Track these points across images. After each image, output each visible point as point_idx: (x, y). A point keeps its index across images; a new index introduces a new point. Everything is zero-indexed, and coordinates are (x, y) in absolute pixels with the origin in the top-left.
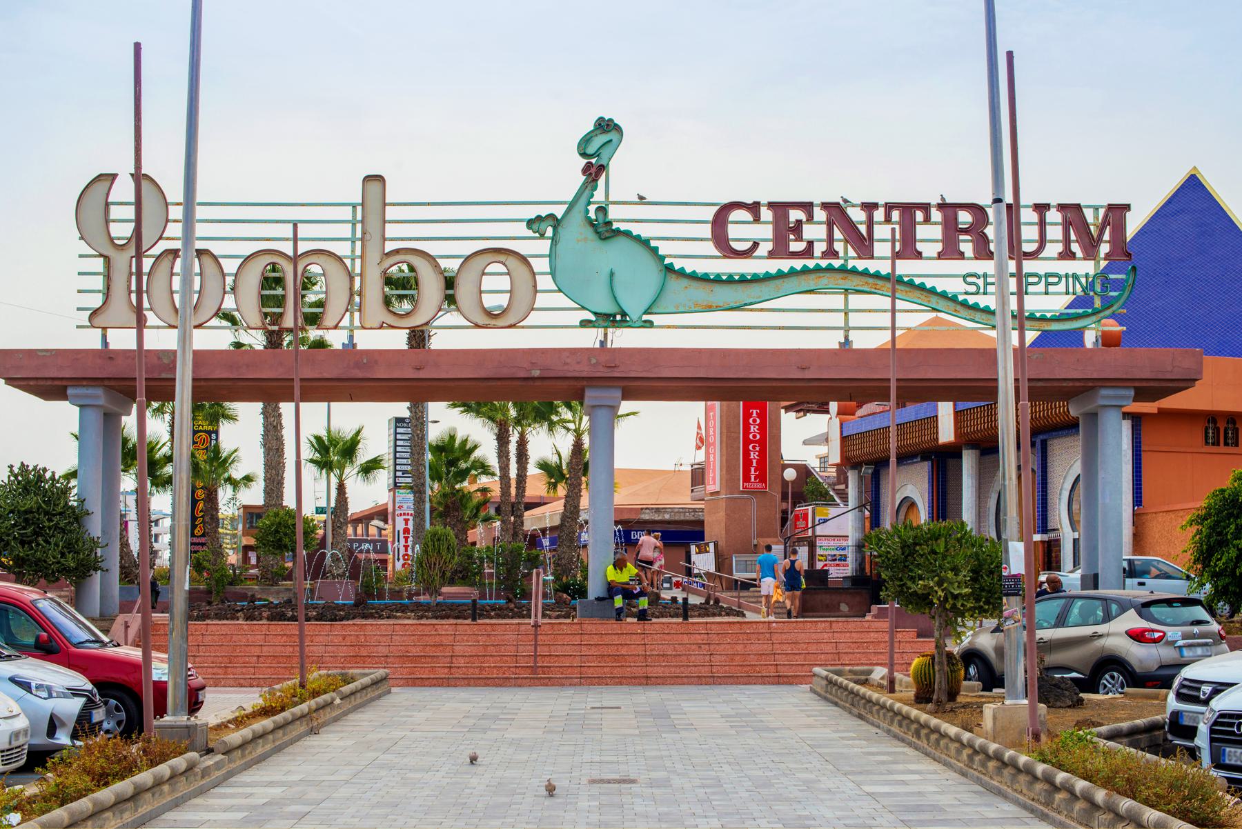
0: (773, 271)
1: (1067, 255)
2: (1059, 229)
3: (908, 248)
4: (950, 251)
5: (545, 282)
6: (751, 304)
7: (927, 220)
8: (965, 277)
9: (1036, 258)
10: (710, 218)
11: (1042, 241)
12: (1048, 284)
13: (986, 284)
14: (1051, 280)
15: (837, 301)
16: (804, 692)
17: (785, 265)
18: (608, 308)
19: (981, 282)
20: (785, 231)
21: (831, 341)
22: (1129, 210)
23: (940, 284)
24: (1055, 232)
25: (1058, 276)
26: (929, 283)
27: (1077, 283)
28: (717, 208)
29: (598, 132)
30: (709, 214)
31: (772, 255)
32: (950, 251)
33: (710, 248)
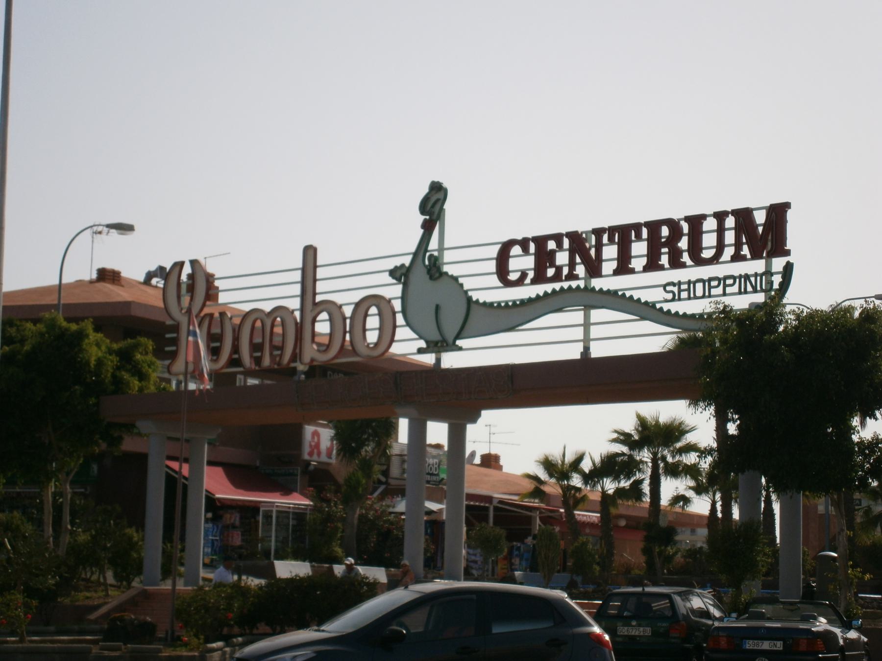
0: (533, 296)
1: (737, 257)
2: (605, 256)
3: (623, 267)
4: (652, 265)
5: (400, 319)
6: (518, 326)
7: (639, 237)
8: (664, 286)
9: (718, 263)
10: (495, 255)
11: (720, 247)
12: (725, 286)
13: (680, 291)
14: (714, 283)
15: (577, 316)
16: (402, 590)
17: (549, 287)
18: (436, 336)
19: (675, 289)
20: (544, 258)
21: (574, 353)
22: (790, 208)
23: (646, 296)
24: (730, 237)
25: (718, 279)
26: (636, 295)
27: (754, 284)
28: (499, 246)
29: (433, 192)
30: (494, 251)
31: (534, 282)
32: (652, 265)
33: (495, 281)
